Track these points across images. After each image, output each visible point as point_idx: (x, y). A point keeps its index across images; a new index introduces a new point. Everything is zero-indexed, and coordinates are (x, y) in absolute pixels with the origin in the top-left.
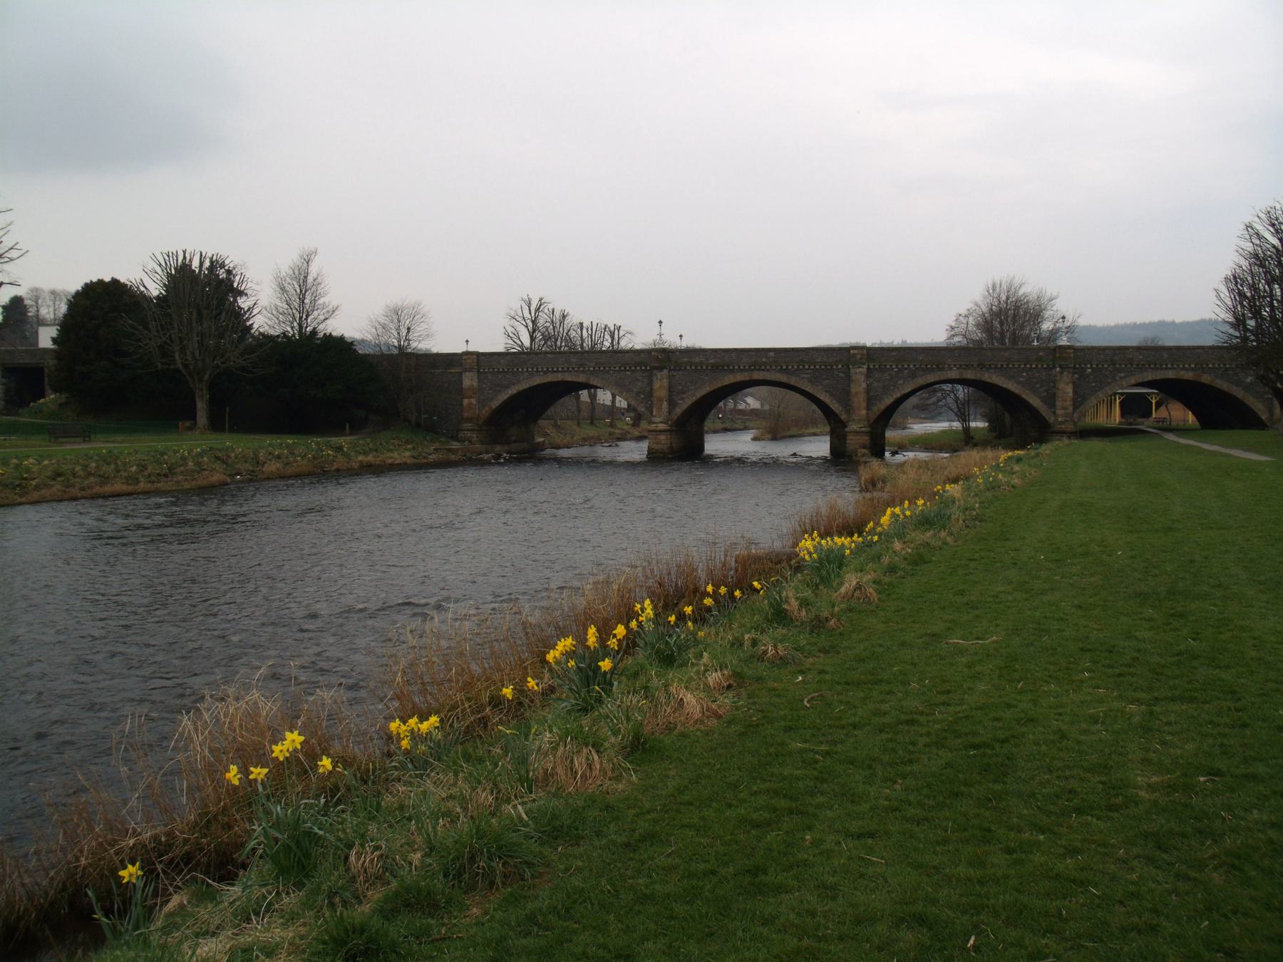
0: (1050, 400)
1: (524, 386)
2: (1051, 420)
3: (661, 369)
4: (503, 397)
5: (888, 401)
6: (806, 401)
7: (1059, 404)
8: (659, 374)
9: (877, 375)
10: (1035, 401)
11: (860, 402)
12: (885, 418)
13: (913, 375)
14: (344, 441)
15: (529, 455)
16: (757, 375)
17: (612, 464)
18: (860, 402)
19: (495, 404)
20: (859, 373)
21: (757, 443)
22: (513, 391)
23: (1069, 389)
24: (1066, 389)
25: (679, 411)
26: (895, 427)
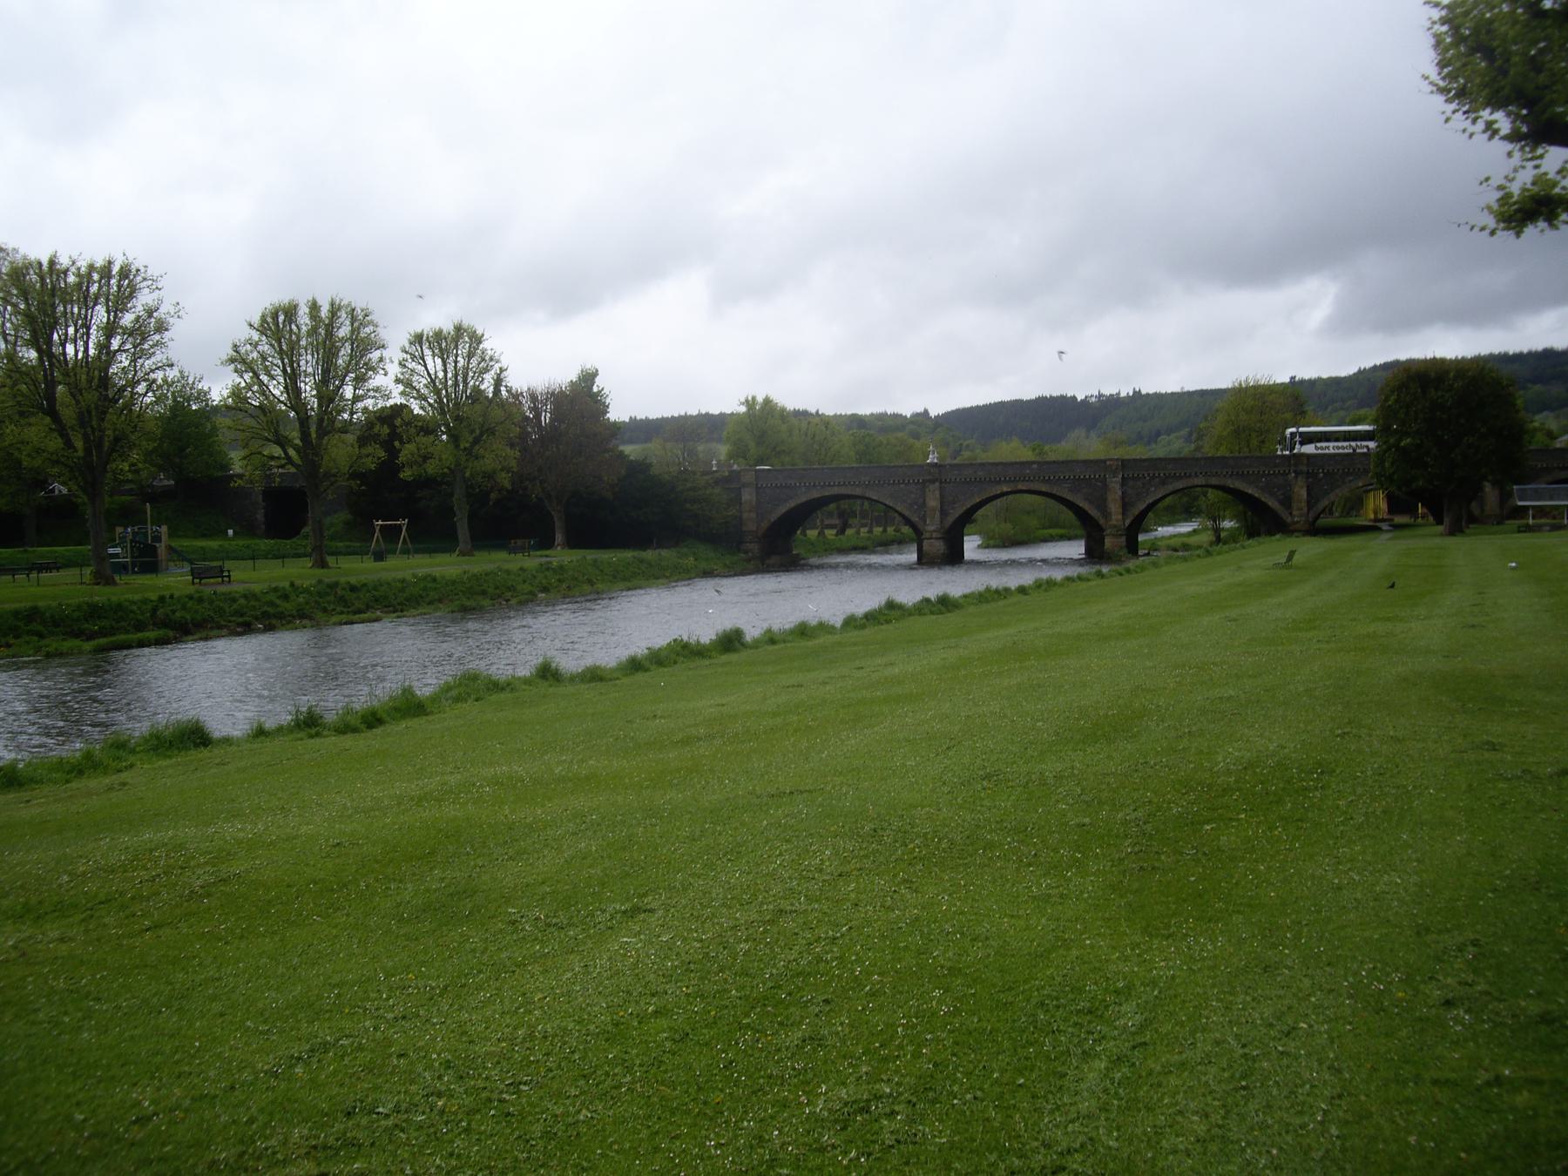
0: (1287, 502)
1: (804, 499)
2: (1289, 520)
3: (933, 482)
4: (782, 510)
5: (1142, 506)
6: (1052, 502)
7: (1295, 506)
8: (932, 487)
9: (1131, 483)
10: (1272, 503)
11: (1114, 508)
12: (1138, 525)
13: (1163, 483)
14: (665, 553)
15: (792, 564)
16: (1020, 487)
17: (883, 566)
18: (1114, 508)
19: (774, 517)
20: (1115, 484)
21: (1534, 232)
22: (792, 504)
23: (1304, 493)
24: (1301, 492)
25: (950, 520)
26: (1147, 531)
